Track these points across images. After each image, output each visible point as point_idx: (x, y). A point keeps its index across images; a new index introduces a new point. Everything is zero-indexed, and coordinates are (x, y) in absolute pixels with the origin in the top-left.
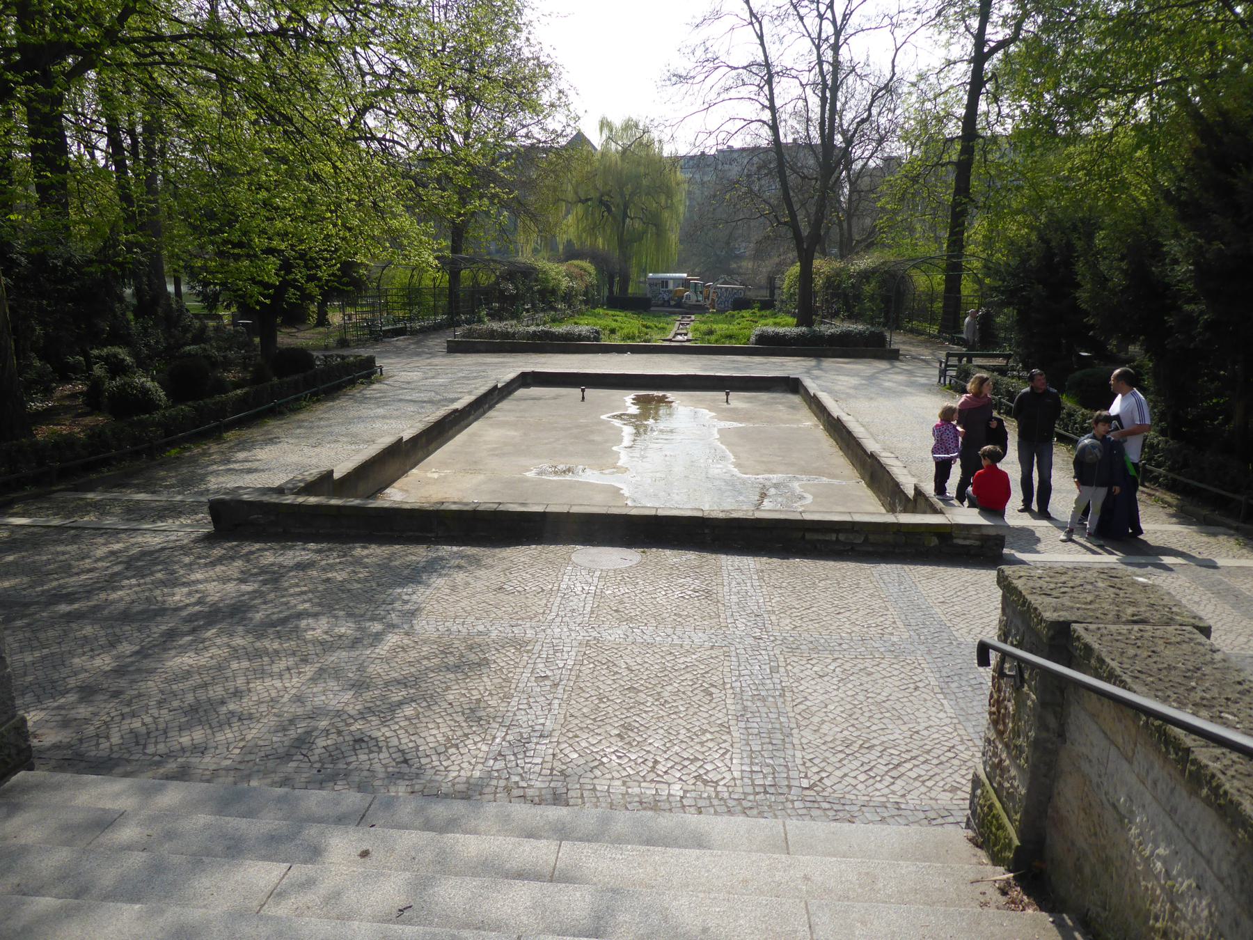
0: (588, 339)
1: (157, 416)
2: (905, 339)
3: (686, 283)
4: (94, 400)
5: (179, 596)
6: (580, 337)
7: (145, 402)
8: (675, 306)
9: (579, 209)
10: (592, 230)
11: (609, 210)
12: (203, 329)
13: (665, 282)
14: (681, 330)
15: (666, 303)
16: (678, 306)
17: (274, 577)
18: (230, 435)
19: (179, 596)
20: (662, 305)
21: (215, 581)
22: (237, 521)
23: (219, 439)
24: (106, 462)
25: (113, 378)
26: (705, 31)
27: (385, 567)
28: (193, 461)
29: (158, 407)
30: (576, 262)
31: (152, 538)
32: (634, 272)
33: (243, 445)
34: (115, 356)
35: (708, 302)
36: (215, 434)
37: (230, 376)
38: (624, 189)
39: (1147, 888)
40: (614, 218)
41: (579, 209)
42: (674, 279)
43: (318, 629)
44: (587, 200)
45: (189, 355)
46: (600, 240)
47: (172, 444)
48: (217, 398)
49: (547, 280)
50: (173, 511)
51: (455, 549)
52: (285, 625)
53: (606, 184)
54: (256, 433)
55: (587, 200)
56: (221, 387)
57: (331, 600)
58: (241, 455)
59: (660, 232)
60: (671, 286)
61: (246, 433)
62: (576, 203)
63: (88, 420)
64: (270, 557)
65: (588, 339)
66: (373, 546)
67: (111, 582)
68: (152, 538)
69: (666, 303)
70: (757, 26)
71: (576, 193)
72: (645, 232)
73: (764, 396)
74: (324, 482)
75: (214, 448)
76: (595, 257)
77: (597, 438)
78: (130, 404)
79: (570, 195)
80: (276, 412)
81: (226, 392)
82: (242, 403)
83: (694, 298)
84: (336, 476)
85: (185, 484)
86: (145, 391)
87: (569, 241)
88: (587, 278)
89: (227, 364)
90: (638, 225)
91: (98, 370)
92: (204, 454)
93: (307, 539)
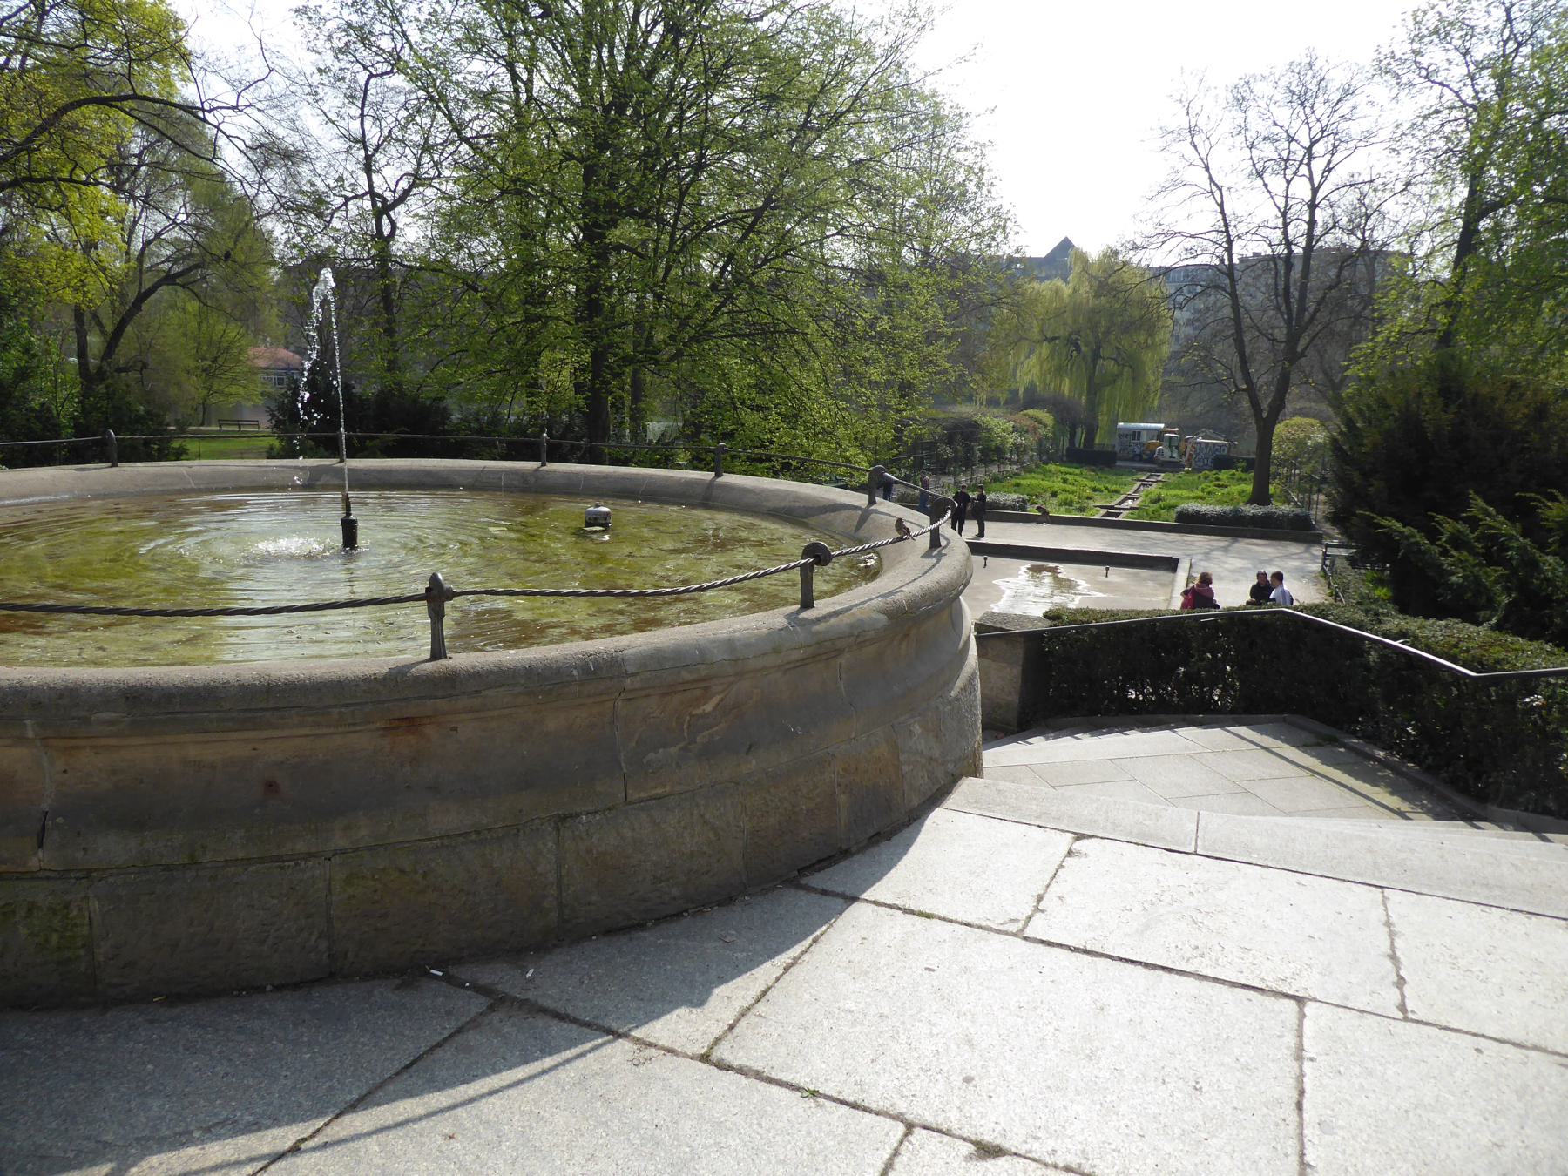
0: (1013, 508)
2: (899, 596)
3: (1160, 435)
6: (1005, 507)
8: (1146, 461)
9: (1045, 349)
10: (1059, 371)
11: (1078, 348)
13: (1137, 434)
14: (1134, 493)
15: (1138, 458)
16: (1145, 459)
20: (1132, 460)
26: (1161, 201)
30: (1030, 412)
32: (1103, 419)
35: (1185, 459)
38: (1107, 314)
40: (1084, 357)
41: (1045, 349)
42: (1148, 430)
44: (1054, 338)
46: (1067, 382)
49: (990, 439)
53: (1075, 321)
55: (1054, 338)
59: (1137, 376)
60: (1144, 438)
62: (1040, 342)
65: (1013, 508)
66: (720, 992)
69: (1138, 458)
70: (1217, 194)
71: (1042, 331)
72: (1120, 374)
73: (1145, 573)
76: (1060, 408)
77: (981, 597)
79: (1035, 333)
83: (1167, 453)
87: (1032, 383)
88: (1042, 431)
90: (1111, 366)
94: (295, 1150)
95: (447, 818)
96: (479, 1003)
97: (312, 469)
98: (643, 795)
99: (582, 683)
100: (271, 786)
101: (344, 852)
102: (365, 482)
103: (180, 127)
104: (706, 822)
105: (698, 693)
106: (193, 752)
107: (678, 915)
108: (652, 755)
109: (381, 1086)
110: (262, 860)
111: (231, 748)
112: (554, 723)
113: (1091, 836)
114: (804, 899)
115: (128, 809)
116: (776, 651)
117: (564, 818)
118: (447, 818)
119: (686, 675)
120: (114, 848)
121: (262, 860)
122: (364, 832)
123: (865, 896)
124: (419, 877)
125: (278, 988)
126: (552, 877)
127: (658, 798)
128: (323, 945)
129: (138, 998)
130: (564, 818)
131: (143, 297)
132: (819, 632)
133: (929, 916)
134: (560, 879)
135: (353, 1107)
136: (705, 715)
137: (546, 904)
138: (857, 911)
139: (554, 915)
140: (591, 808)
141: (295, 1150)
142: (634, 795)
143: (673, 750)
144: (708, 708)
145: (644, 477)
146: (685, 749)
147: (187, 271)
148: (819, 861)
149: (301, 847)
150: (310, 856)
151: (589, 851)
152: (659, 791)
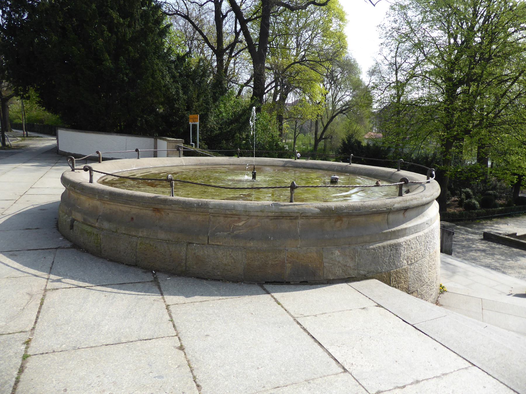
1: (476, 211)
4: (460, 203)
5: (474, 246)
7: (473, 207)
12: (496, 185)
17: (494, 248)
18: (495, 220)
19: (474, 246)
21: (482, 246)
22: (488, 237)
23: (491, 220)
24: (462, 220)
25: (467, 199)
27: (517, 253)
28: (483, 224)
29: (476, 209)
31: (470, 236)
33: (497, 223)
34: (468, 192)
36: (490, 218)
37: (500, 202)
39: (442, 8)
43: (498, 257)
45: (490, 195)
47: (478, 219)
48: (493, 209)
50: (475, 233)
51: (518, 250)
52: (493, 254)
54: (503, 221)
56: (496, 206)
57: (502, 254)
58: (496, 225)
61: (499, 220)
63: (458, 209)
64: (494, 245)
67: (463, 241)
68: (470, 236)
74: (514, 235)
75: (489, 222)
78: (470, 207)
80: (511, 216)
81: (497, 207)
82: (501, 211)
84: (517, 235)
85: (479, 229)
86: (474, 204)
89: (500, 198)
91: (463, 196)
92: (486, 223)
93: (503, 244)
94: (84, 287)
95: (162, 235)
96: (152, 278)
97: (286, 161)
98: (213, 243)
99: (197, 208)
100: (132, 219)
101: (141, 237)
102: (342, 171)
103: (349, 67)
104: (231, 257)
105: (237, 219)
106: (121, 208)
107: (219, 280)
108: (218, 233)
109: (111, 285)
110: (127, 235)
111: (125, 208)
112: (192, 218)
113: (382, 307)
114: (258, 288)
115: (109, 218)
116: (262, 211)
117: (190, 243)
118: (162, 235)
119: (228, 212)
120: (106, 225)
121: (127, 235)
122: (145, 233)
123: (273, 294)
124: (154, 248)
125: (126, 264)
126: (184, 257)
127: (218, 245)
128: (135, 258)
129: (105, 258)
130: (190, 243)
131: (333, 117)
132: (281, 209)
133: (279, 304)
134: (186, 259)
135: (103, 286)
136: (239, 226)
137: (182, 264)
138: (268, 296)
139: (184, 268)
140: (197, 242)
141: (84, 287)
142: (210, 242)
143: (225, 233)
144: (240, 224)
145: (376, 170)
146: (229, 234)
147: (347, 109)
148: (274, 282)
149: (134, 233)
150: (135, 236)
151: (195, 254)
152: (218, 243)
